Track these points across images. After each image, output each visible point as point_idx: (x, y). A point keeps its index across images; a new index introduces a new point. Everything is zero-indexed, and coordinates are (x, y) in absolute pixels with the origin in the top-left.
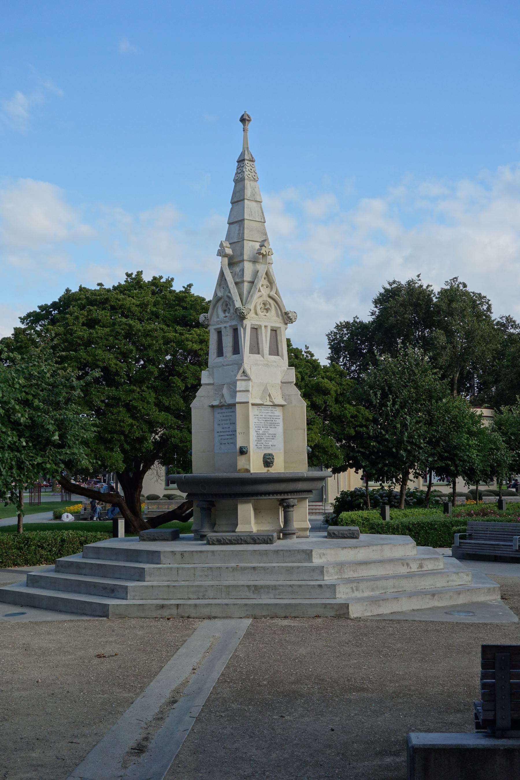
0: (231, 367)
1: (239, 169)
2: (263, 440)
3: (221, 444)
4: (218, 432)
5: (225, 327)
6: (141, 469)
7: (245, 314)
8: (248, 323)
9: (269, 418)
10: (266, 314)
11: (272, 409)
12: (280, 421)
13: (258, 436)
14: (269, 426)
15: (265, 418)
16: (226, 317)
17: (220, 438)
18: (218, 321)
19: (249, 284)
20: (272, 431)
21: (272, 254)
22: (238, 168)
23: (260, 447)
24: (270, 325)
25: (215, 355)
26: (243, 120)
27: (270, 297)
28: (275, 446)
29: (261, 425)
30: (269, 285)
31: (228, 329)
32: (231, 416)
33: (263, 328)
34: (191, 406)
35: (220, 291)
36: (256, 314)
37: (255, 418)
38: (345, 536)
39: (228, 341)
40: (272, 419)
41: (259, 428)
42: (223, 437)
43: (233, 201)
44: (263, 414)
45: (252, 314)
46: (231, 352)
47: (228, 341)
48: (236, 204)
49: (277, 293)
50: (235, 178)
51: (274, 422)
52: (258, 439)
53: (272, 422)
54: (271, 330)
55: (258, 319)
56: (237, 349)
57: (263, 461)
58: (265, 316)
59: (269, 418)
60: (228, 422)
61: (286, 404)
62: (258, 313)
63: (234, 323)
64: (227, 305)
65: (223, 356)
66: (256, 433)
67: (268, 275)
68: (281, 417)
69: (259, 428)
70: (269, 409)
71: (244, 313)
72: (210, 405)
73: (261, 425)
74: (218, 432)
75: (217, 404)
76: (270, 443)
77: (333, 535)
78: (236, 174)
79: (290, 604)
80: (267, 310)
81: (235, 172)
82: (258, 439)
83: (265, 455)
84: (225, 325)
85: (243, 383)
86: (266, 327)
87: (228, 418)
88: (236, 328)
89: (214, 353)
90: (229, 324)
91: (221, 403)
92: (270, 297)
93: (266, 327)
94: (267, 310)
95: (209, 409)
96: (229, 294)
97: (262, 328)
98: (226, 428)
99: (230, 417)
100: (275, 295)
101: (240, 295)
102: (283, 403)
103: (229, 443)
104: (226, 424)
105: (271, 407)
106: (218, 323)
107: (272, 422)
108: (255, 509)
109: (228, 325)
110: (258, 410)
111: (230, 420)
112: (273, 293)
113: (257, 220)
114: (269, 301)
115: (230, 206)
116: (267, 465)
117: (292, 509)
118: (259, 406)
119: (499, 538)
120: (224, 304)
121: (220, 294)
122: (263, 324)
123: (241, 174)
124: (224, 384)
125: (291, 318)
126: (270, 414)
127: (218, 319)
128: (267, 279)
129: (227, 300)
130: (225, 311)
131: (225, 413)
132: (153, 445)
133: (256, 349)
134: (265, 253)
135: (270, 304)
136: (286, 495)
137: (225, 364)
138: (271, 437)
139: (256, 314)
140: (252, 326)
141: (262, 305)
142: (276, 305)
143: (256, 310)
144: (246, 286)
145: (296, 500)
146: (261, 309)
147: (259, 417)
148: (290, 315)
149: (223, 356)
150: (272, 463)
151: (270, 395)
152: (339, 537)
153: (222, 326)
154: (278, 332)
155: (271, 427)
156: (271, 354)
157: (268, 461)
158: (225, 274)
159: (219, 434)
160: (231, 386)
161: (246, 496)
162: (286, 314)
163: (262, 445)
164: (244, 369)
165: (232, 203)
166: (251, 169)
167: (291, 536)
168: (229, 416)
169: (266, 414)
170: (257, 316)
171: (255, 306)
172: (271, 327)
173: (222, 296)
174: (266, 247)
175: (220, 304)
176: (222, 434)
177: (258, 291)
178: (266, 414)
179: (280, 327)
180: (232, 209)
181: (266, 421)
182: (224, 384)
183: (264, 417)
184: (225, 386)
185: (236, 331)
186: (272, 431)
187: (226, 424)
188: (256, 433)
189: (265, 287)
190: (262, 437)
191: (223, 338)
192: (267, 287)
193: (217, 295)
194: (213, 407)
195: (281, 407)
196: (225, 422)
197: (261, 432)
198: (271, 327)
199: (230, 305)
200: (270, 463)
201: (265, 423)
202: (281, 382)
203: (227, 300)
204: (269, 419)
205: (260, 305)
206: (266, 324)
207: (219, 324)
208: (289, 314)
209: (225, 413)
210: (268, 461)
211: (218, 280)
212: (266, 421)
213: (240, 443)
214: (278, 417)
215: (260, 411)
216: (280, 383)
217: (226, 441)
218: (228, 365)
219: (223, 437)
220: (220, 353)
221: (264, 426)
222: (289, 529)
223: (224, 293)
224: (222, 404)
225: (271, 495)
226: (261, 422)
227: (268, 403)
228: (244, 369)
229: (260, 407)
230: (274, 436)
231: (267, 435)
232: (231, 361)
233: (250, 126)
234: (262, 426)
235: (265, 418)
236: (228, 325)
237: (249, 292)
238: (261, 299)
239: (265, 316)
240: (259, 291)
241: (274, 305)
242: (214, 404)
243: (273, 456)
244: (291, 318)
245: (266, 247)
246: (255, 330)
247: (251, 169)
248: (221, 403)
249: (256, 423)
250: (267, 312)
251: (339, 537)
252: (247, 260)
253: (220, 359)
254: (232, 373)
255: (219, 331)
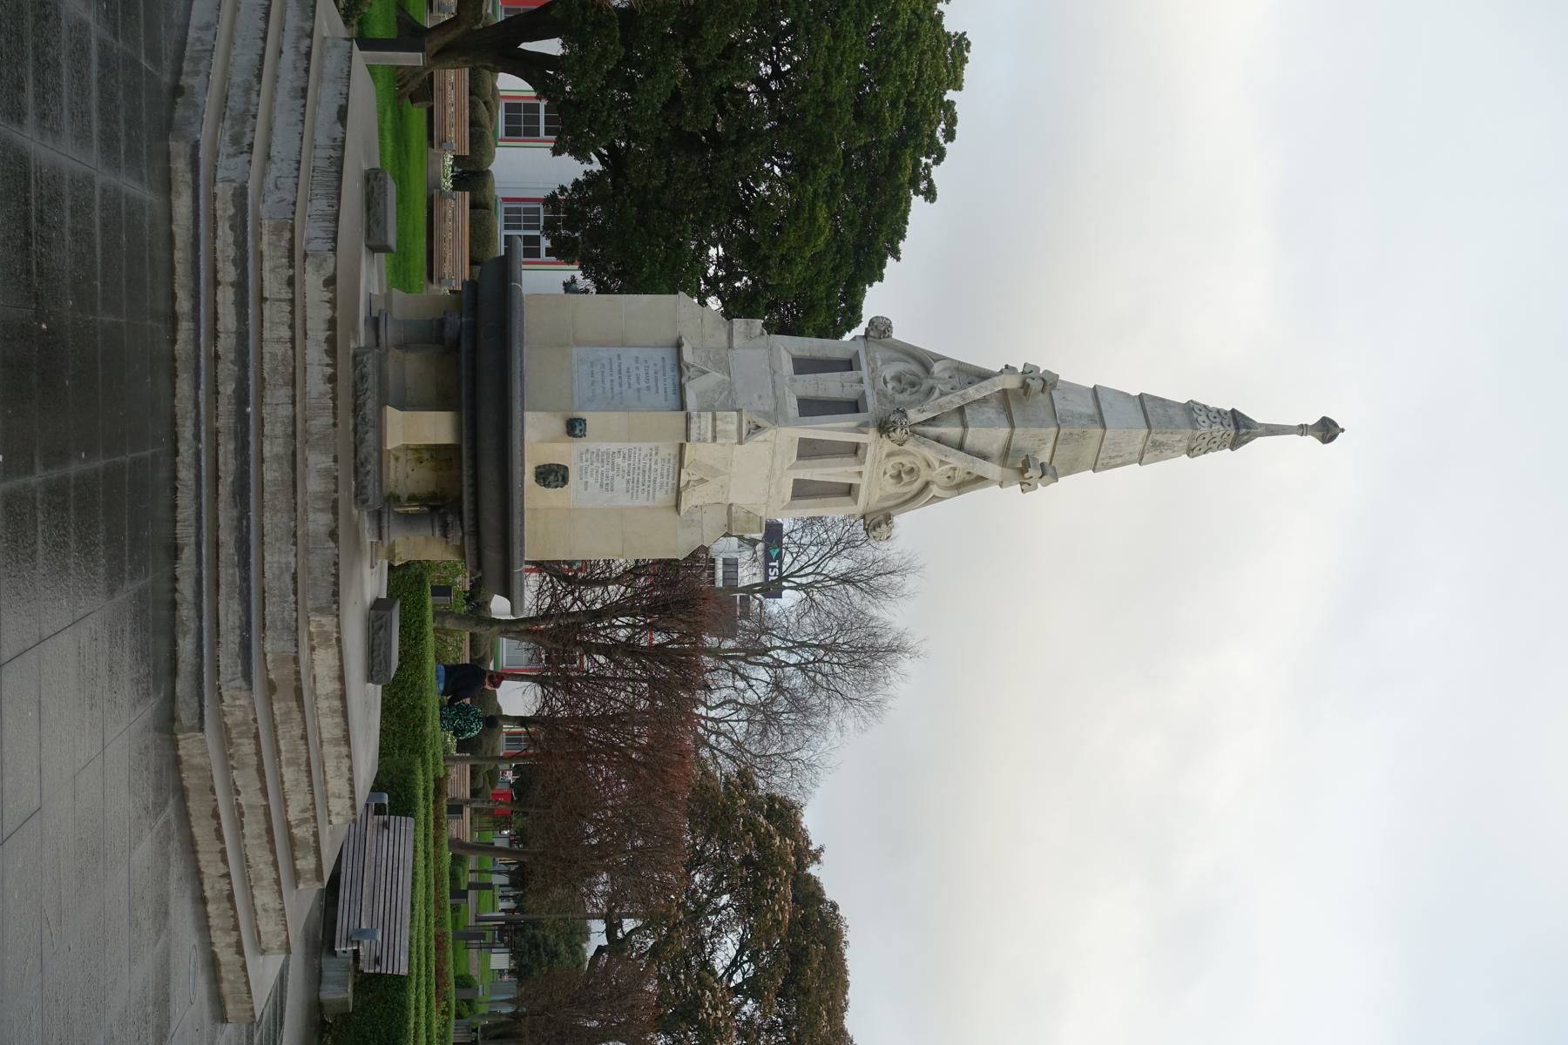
0: (770, 393)
1: (1217, 415)
2: (599, 465)
3: (592, 364)
4: (619, 356)
5: (861, 381)
6: (525, 46)
7: (892, 434)
8: (870, 438)
9: (649, 477)
10: (888, 475)
11: (670, 485)
12: (641, 501)
13: (608, 454)
14: (631, 477)
15: (650, 469)
16: (885, 383)
17: (606, 362)
18: (875, 363)
19: (958, 440)
20: (620, 484)
21: (1023, 490)
22: (1218, 411)
23: (584, 458)
24: (863, 484)
25: (798, 353)
26: (1327, 430)
27: (927, 484)
28: (586, 489)
29: (634, 461)
30: (955, 482)
31: (857, 387)
32: (657, 392)
33: (857, 469)
34: (681, 293)
35: (945, 370)
36: (889, 455)
37: (651, 449)
38: (375, 653)
39: (831, 385)
40: (647, 483)
41: (627, 457)
42: (607, 370)
43: (1145, 399)
44: (659, 466)
45: (888, 445)
46: (804, 394)
47: (831, 385)
48: (1139, 408)
49: (936, 499)
50: (1197, 404)
51: (641, 487)
52: (603, 455)
53: (641, 484)
54: (851, 484)
55: (878, 458)
56: (811, 407)
57: (550, 465)
58: (885, 473)
59: (649, 477)
60: (643, 385)
61: (682, 514)
62: (892, 459)
63: (871, 402)
64: (913, 385)
65: (795, 374)
66: (616, 451)
67: (980, 480)
68: (650, 503)
69: (627, 457)
70: (671, 479)
71: (894, 430)
72: (684, 340)
73: (634, 461)
74: (619, 356)
75: (685, 358)
76: (591, 481)
77: (377, 625)
78: (1205, 406)
79: (247, 292)
80: (898, 477)
81: (1211, 406)
82: (603, 455)
83: (566, 468)
84: (866, 380)
85: (733, 428)
86: (860, 473)
87: (652, 384)
88: (854, 368)
89: (803, 350)
90: (869, 392)
91: (688, 368)
92: (927, 484)
93: (860, 473)
94: (898, 477)
95: (671, 337)
96: (937, 393)
97: (858, 467)
98: (629, 377)
99: (653, 390)
100: (932, 495)
101: (934, 418)
102: (684, 507)
103: (593, 384)
104: (638, 378)
105: (675, 481)
106: (872, 361)
107: (641, 484)
108: (436, 450)
109: (867, 386)
110: (669, 454)
111: (648, 388)
112: (935, 490)
113: (1101, 455)
114: (918, 481)
115: (1135, 393)
116: (541, 473)
117: (437, 533)
118: (678, 458)
119: (377, 893)
120: (913, 378)
121: (937, 368)
122: (866, 468)
123: (1206, 420)
124: (730, 377)
125: (878, 529)
126: (658, 480)
127: (879, 363)
128: (968, 478)
129: (925, 387)
130: (898, 378)
131: (664, 375)
132: (596, 287)
133: (809, 450)
134: (1026, 475)
135: (910, 483)
136: (473, 529)
137: (776, 377)
138: (605, 482)
139: (889, 455)
140: (862, 446)
141: (908, 466)
142: (907, 497)
143: (898, 455)
144: (951, 431)
145: (458, 543)
146: (901, 463)
147: (654, 458)
148: (884, 526)
149: (795, 374)
150: (547, 485)
151: (702, 481)
152: (373, 640)
153: (865, 372)
154: (847, 499)
155: (628, 482)
156: (796, 481)
157: (553, 475)
158: (984, 383)
159: (615, 359)
160: (726, 392)
161: (470, 428)
162: (888, 519)
163: (589, 463)
164: (766, 428)
165: (1141, 396)
166: (1215, 442)
167: (376, 532)
168: (657, 385)
169: (659, 472)
170: (884, 455)
171: (907, 453)
172: (859, 485)
173: (933, 373)
174: (1041, 477)
175: (915, 368)
176: (615, 365)
177: (941, 461)
178: (659, 472)
179: (856, 503)
180: (1128, 395)
181: (644, 471)
182: (730, 377)
183: (653, 466)
184: (727, 378)
185: (854, 406)
186: (620, 484)
187: (638, 378)
188: (616, 451)
189: (950, 474)
190: (606, 462)
191: (837, 374)
192: (949, 477)
193: (935, 361)
194: (679, 346)
195: (673, 503)
196: (643, 377)
197: (619, 461)
198: (859, 485)
199: (911, 394)
200: (544, 480)
201: (639, 468)
202: (731, 505)
203: (925, 387)
204: (647, 477)
205: (910, 463)
206: (866, 476)
207: (868, 364)
208: (887, 524)
209: (664, 375)
210: (553, 475)
211: (971, 365)
212: (644, 471)
213: (593, 419)
214: (651, 496)
215: (666, 461)
216: (730, 502)
217: (598, 377)
218: (774, 387)
219: (607, 370)
220: (803, 366)
221: (632, 466)
222: (391, 528)
223: (940, 379)
224: (685, 369)
225: (471, 472)
226: (642, 461)
227: (684, 478)
228: (766, 428)
229: (675, 458)
230: (608, 487)
231: (611, 473)
232: (784, 394)
233: (1311, 441)
234: (632, 462)
235: (650, 469)
236: (867, 386)
237: (938, 440)
238: (922, 466)
239: (885, 473)
240: (942, 463)
241: (906, 493)
242: (684, 348)
243: (562, 487)
244: (878, 529)
245: (1041, 477)
246: (855, 450)
247: (1215, 442)
248: (688, 368)
249: (640, 450)
250: (892, 477)
251: (373, 640)
252: (1012, 434)
253: (788, 367)
254: (755, 396)
255: (860, 404)
